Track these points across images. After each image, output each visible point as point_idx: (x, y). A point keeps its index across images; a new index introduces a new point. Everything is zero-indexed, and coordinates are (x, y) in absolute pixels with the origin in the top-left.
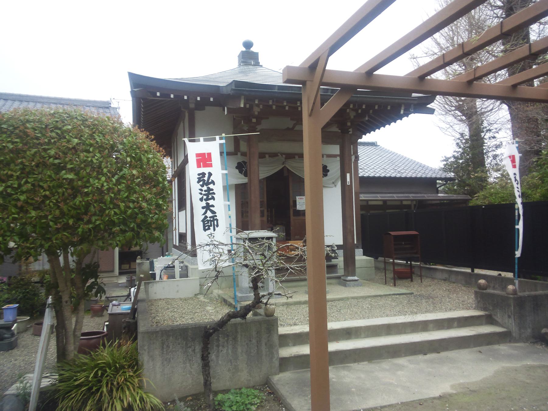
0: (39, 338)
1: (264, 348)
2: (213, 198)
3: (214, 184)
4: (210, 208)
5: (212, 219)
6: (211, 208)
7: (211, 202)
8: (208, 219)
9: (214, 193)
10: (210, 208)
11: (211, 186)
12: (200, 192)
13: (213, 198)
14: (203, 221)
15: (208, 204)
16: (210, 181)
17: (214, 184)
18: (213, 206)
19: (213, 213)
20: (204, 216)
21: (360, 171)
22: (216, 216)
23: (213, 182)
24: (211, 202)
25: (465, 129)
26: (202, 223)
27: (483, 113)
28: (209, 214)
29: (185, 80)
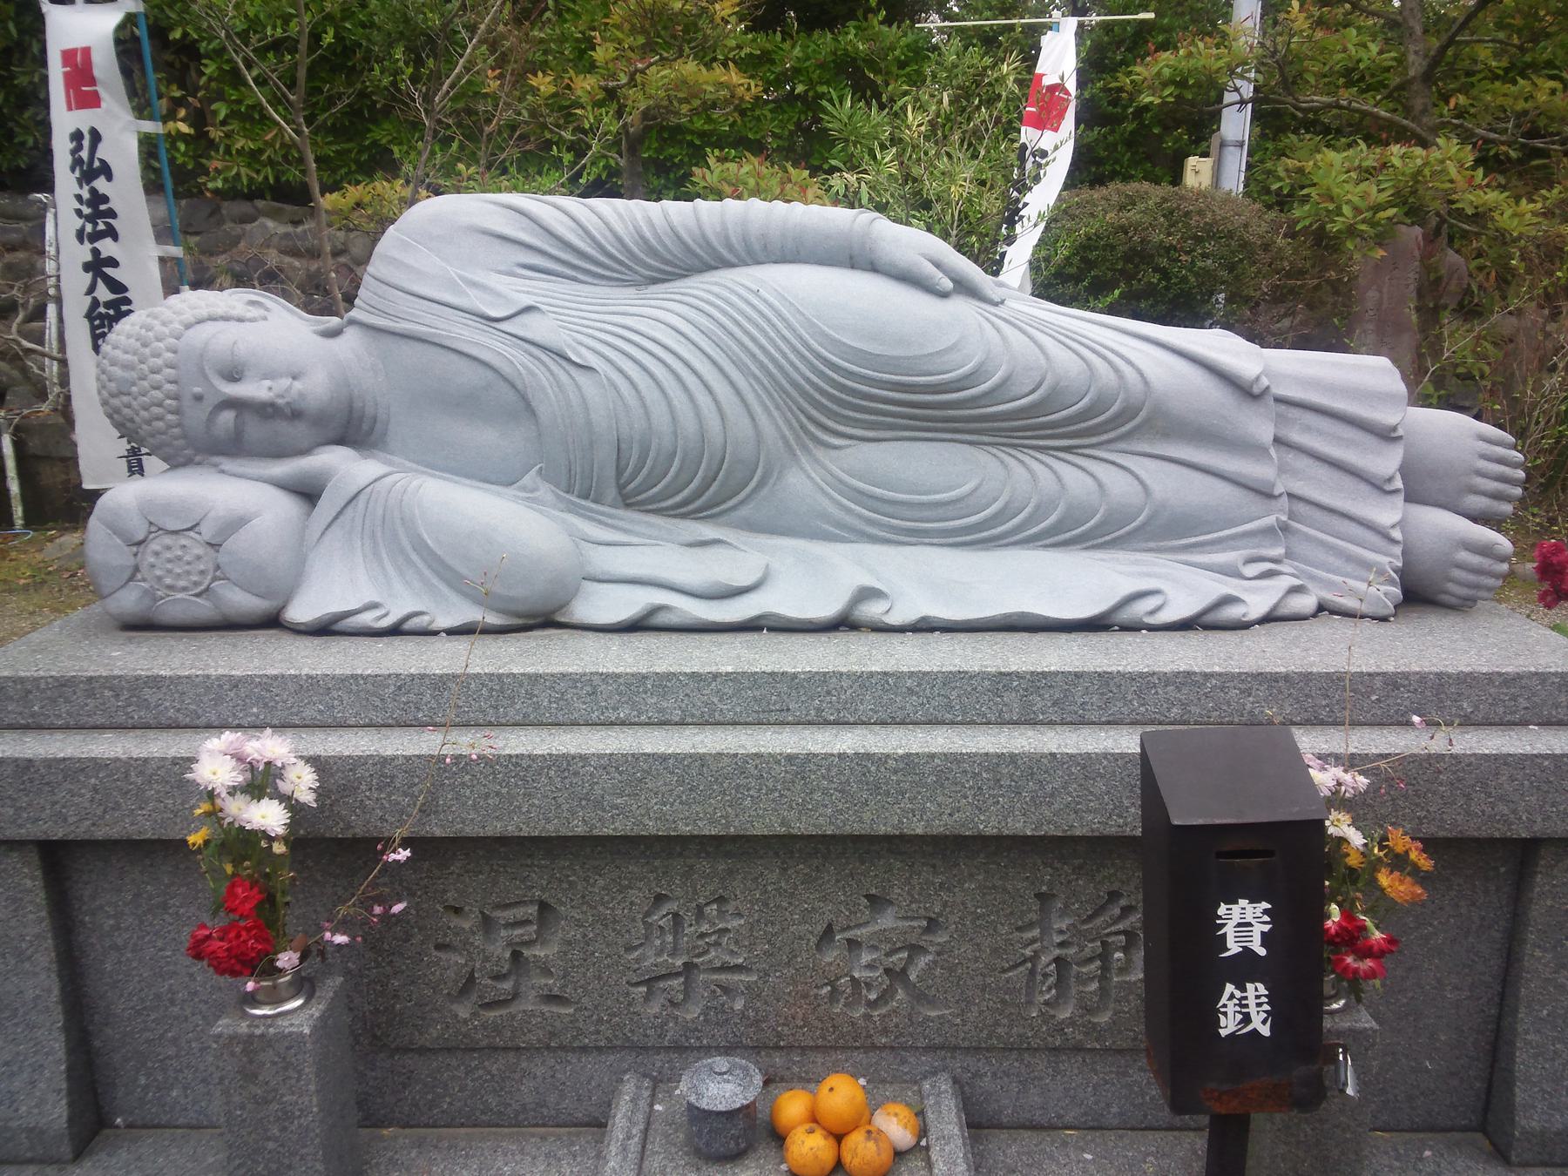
0: (71, 539)
1: (611, 407)
2: (112, 233)
3: (109, 178)
4: (105, 269)
5: (111, 312)
6: (109, 271)
7: (107, 247)
8: (102, 310)
9: (112, 214)
10: (105, 269)
11: (101, 184)
12: (78, 206)
13: (112, 233)
14: (90, 316)
15: (96, 252)
16: (97, 164)
17: (109, 178)
18: (113, 263)
19: (113, 292)
20: (88, 299)
21: (1128, 831)
22: (128, 302)
23: (106, 170)
24: (107, 247)
25: (269, 731)
26: (86, 322)
27: (252, 767)
28: (104, 294)
29: (857, 420)
